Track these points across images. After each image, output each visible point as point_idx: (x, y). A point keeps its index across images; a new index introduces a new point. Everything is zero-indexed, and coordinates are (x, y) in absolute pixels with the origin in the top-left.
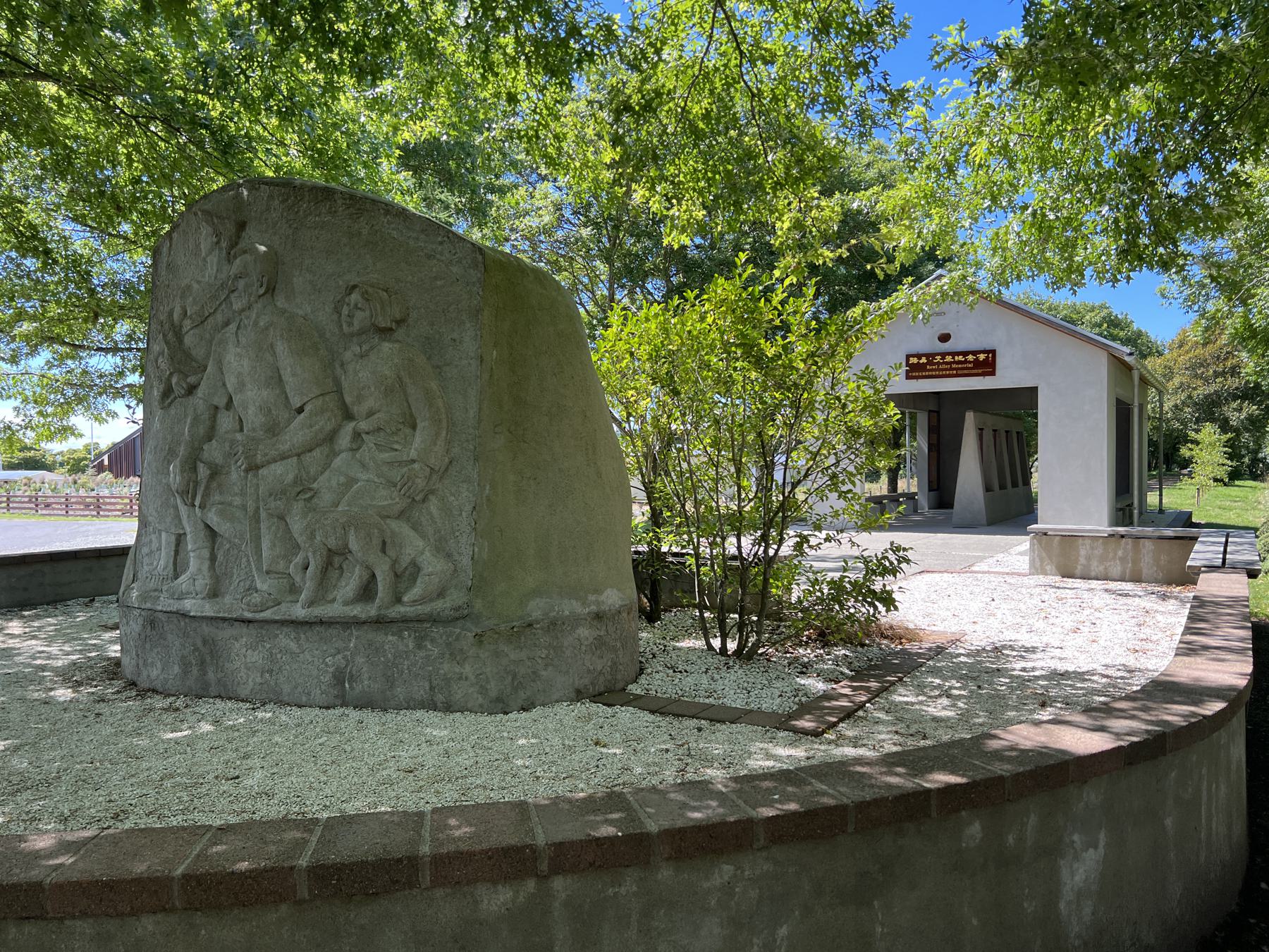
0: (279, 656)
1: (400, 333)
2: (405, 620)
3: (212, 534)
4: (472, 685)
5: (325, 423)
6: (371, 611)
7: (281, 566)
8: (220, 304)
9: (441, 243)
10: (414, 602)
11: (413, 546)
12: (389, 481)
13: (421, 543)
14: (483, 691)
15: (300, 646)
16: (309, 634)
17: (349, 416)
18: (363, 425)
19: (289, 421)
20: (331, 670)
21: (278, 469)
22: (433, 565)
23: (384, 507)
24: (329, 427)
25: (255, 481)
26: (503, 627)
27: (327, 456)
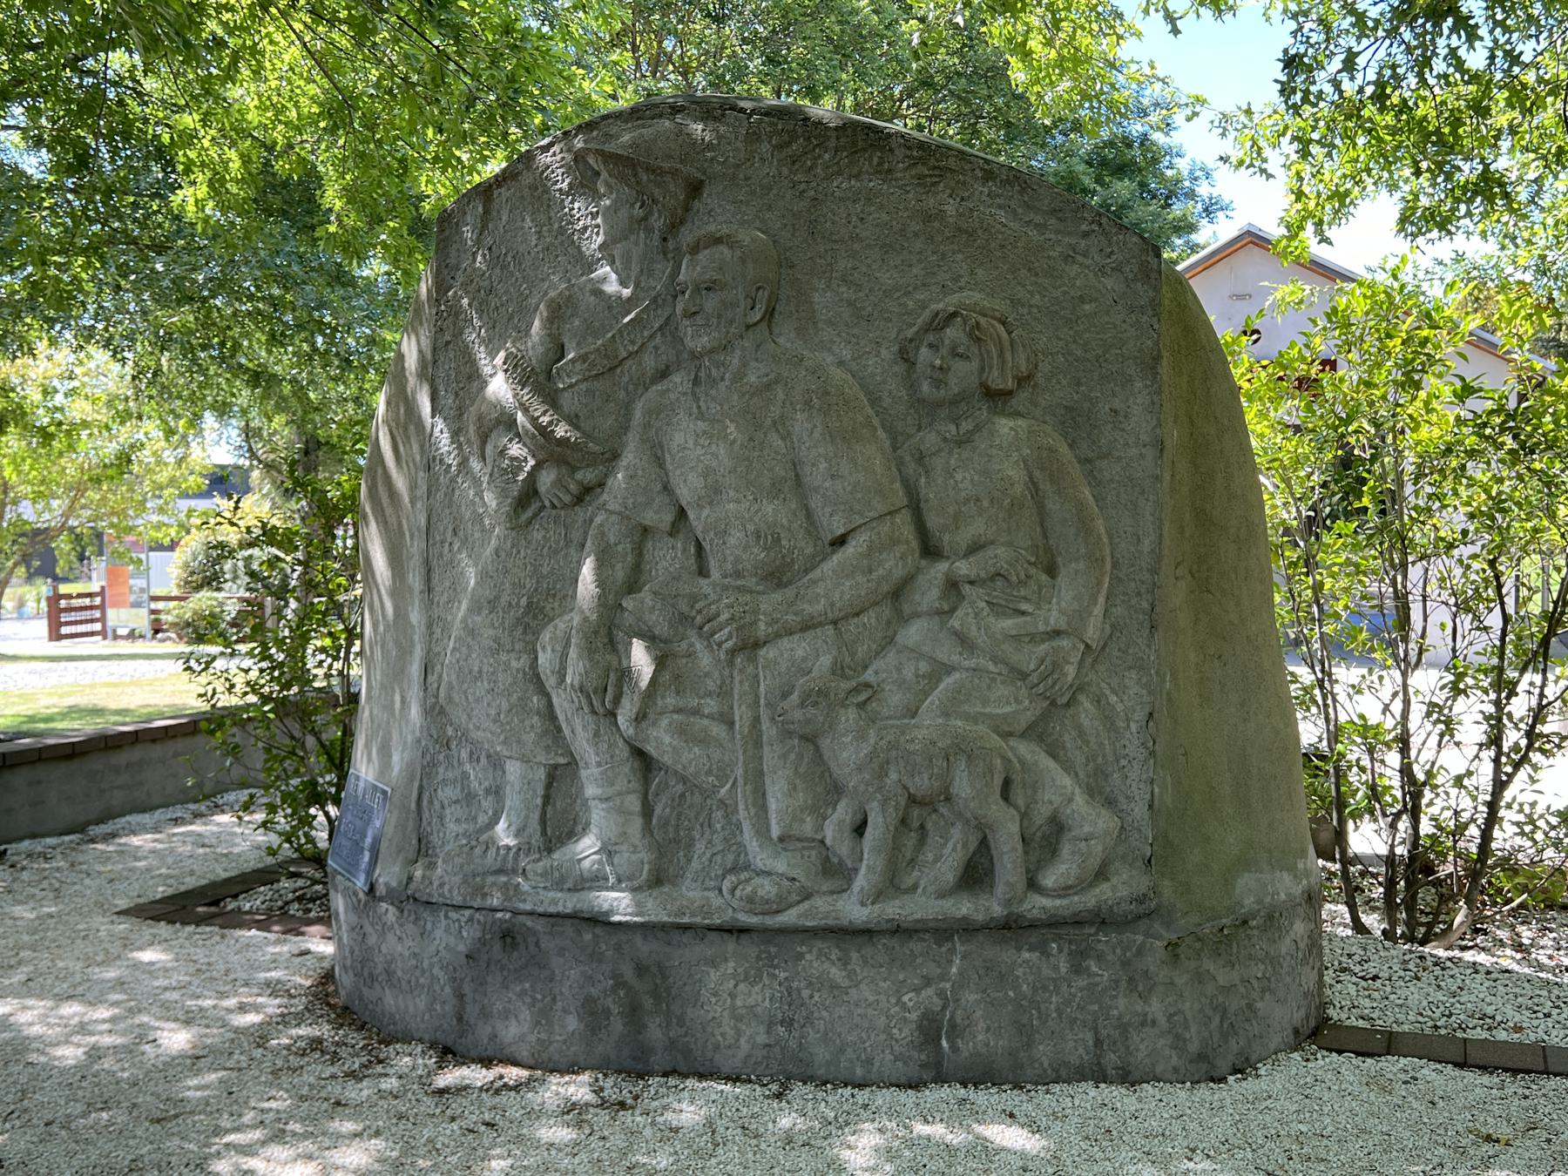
0: (805, 993)
1: (1021, 400)
2: (1054, 924)
3: (644, 761)
4: (1162, 1035)
5: (892, 566)
6: (991, 906)
7: (808, 828)
8: (651, 337)
9: (1086, 235)
10: (1065, 891)
11: (1059, 787)
12: (1013, 669)
13: (1066, 781)
14: (1179, 1042)
15: (851, 975)
16: (868, 951)
17: (930, 550)
18: (963, 568)
19: (813, 563)
20: (914, 1016)
21: (796, 648)
22: (1091, 822)
23: (1005, 717)
24: (899, 572)
25: (750, 669)
26: (1207, 929)
27: (889, 623)
